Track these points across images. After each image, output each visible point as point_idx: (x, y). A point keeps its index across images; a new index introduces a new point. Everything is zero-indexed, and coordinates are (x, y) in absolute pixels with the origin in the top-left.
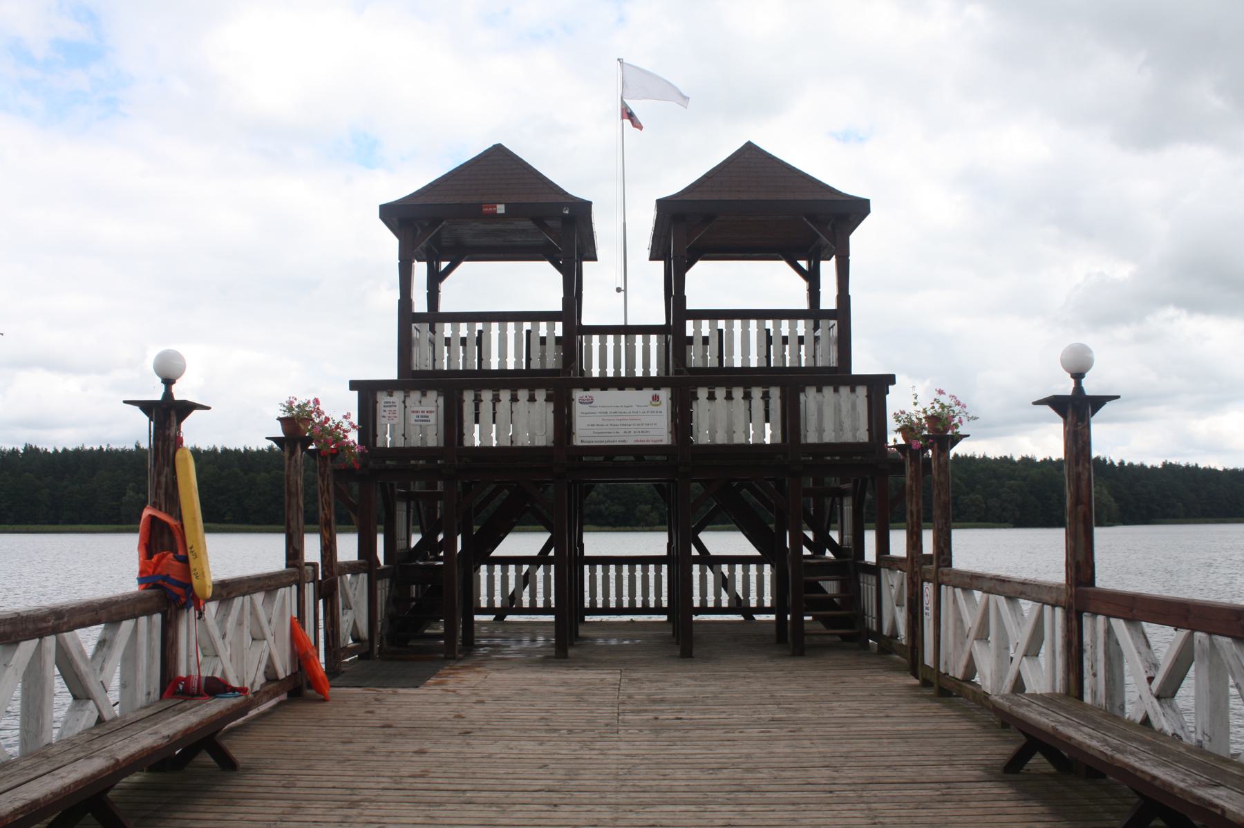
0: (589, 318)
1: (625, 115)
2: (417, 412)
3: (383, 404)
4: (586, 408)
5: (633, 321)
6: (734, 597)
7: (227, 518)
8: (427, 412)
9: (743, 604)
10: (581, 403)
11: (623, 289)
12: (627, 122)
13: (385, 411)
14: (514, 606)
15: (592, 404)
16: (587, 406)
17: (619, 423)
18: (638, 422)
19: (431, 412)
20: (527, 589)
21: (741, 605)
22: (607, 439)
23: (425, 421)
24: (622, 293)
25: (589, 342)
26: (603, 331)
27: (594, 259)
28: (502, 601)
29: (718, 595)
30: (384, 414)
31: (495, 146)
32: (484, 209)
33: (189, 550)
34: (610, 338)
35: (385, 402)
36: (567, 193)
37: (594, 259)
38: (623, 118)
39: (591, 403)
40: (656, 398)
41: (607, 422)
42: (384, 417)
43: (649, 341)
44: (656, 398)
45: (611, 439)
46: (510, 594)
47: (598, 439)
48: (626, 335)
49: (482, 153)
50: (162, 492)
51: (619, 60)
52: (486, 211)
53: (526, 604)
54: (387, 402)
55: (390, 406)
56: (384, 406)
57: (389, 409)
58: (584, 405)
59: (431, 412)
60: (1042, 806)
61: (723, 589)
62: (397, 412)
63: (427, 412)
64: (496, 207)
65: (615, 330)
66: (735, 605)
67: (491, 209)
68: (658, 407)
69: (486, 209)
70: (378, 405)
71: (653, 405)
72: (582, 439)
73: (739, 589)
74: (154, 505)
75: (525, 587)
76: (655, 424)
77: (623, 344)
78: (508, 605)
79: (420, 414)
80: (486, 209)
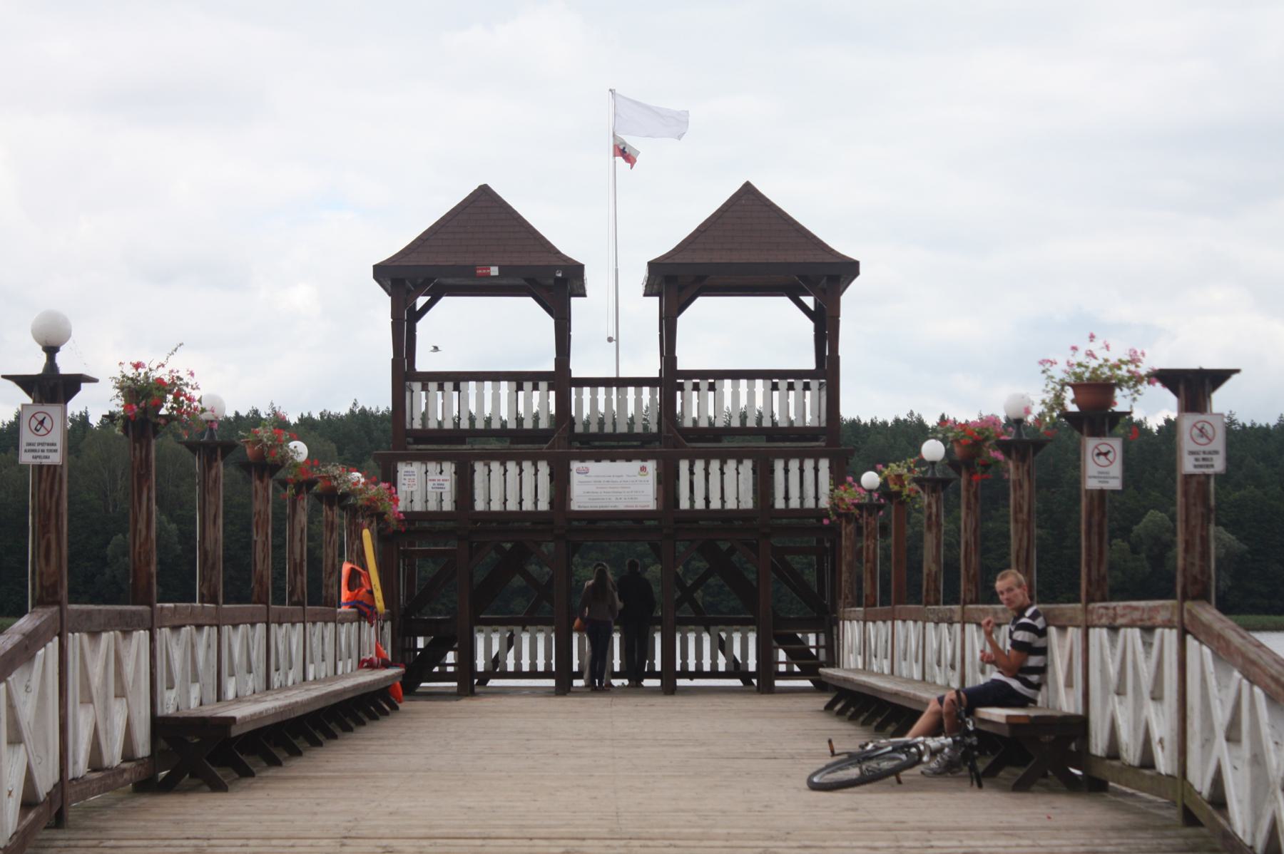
0: (577, 371)
1: (618, 152)
2: (434, 480)
3: (403, 473)
4: (582, 477)
5: (624, 374)
6: (732, 661)
8: (443, 480)
9: (742, 668)
10: (578, 473)
11: (614, 338)
12: (620, 160)
13: (405, 479)
14: (498, 670)
15: (588, 474)
16: (583, 475)
17: (611, 490)
18: (628, 490)
19: (446, 480)
20: (512, 650)
21: (739, 669)
22: (601, 504)
23: (441, 488)
24: (614, 343)
25: (579, 395)
26: (594, 383)
27: (583, 294)
28: (485, 664)
29: (714, 658)
30: (404, 482)
31: (480, 187)
32: (477, 272)
33: (373, 587)
34: (601, 390)
35: (405, 472)
36: (558, 252)
37: (583, 294)
38: (615, 156)
39: (587, 473)
40: (643, 469)
41: (602, 490)
42: (404, 484)
43: (641, 393)
44: (643, 469)
45: (604, 504)
46: (493, 657)
47: (592, 505)
48: (618, 387)
49: (468, 197)
50: (355, 555)
51: (611, 90)
52: (481, 273)
53: (511, 668)
54: (407, 472)
55: (410, 475)
56: (405, 475)
57: (409, 477)
58: (580, 475)
59: (446, 480)
60: (856, 730)
61: (719, 652)
62: (416, 481)
63: (443, 480)
64: (489, 269)
65: (607, 383)
66: (732, 669)
67: (484, 271)
68: (645, 477)
69: (480, 271)
70: (399, 474)
71: (641, 475)
72: (579, 504)
73: (737, 652)
74: (350, 561)
75: (497, 655)
76: (643, 492)
77: (614, 397)
78: (491, 669)
79: (436, 482)
80: (480, 271)
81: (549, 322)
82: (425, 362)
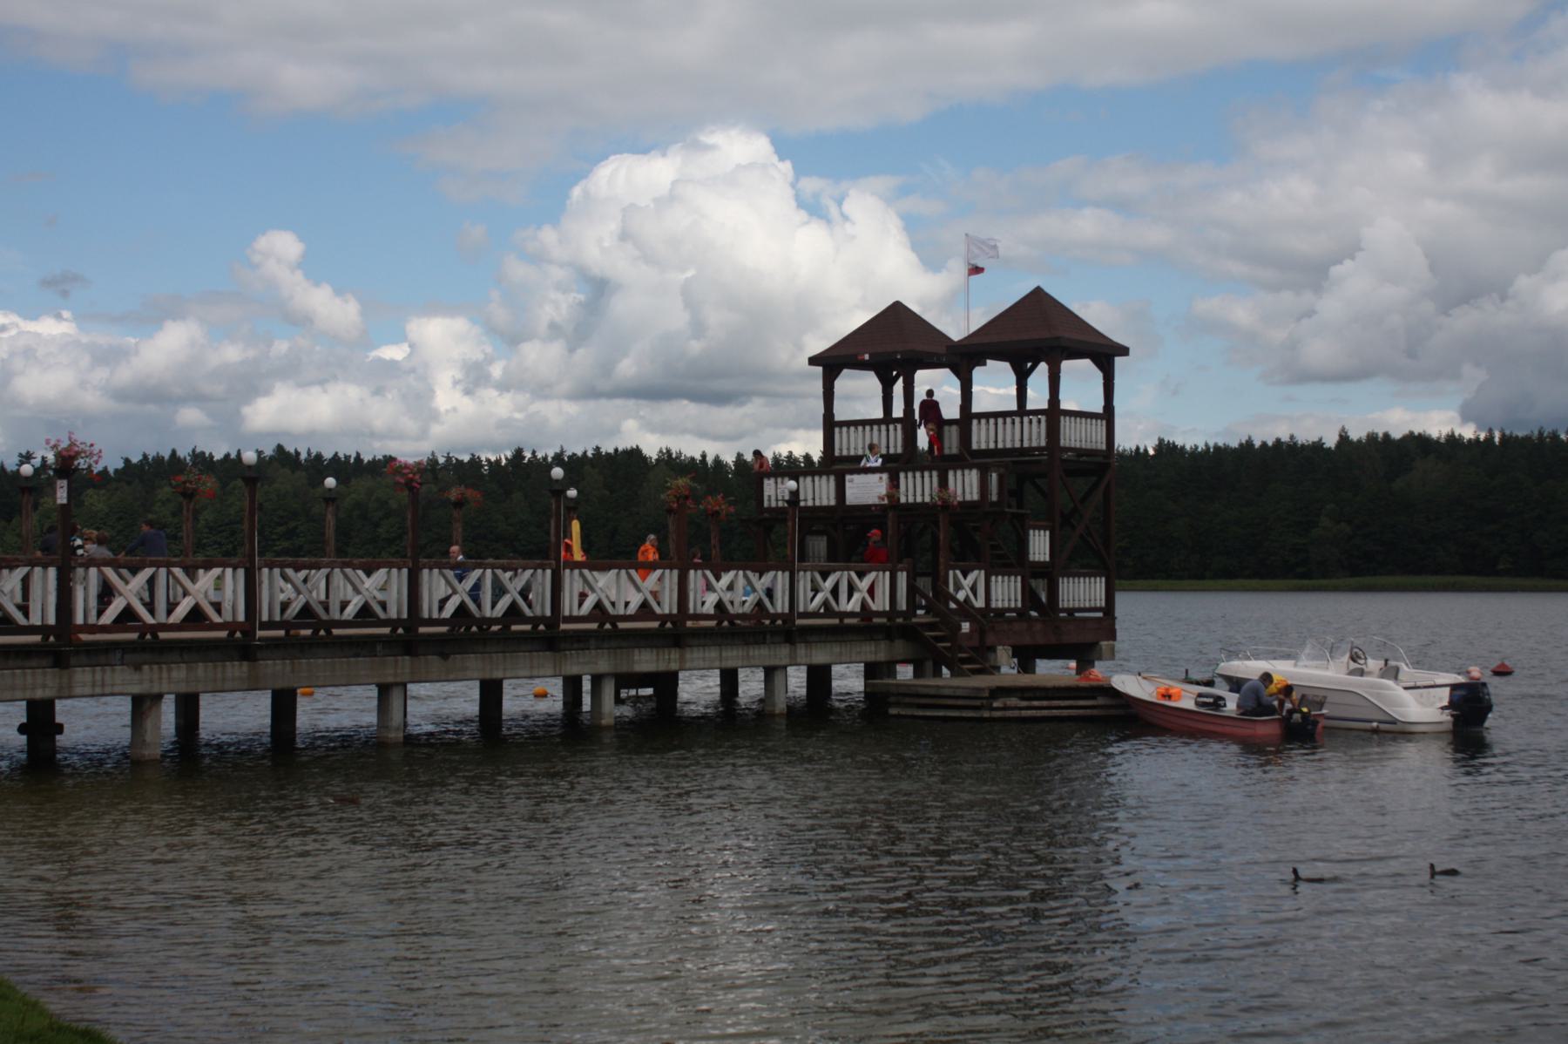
7: (1501, 567)
81: (1098, 376)
82: (840, 414)
